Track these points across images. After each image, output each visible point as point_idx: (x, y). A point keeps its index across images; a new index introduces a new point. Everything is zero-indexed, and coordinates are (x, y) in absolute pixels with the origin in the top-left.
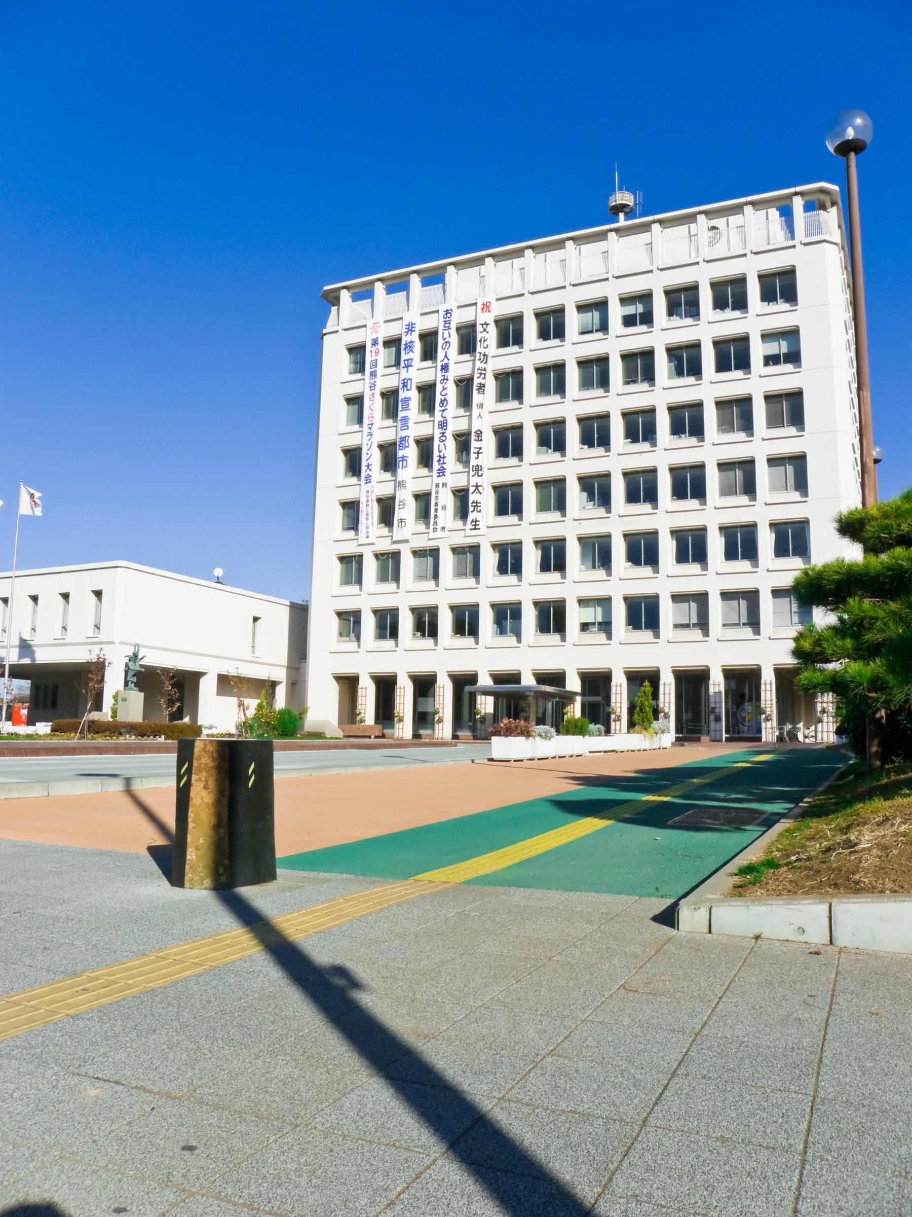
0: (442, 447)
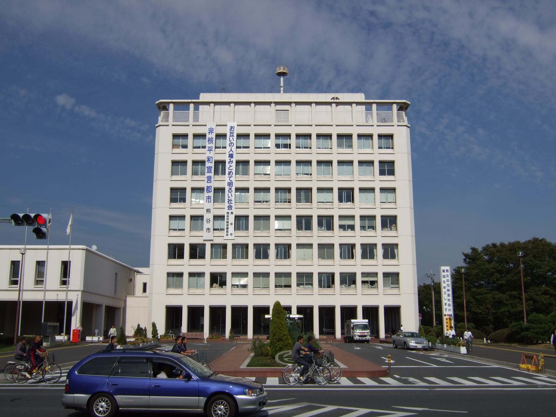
0: (230, 195)
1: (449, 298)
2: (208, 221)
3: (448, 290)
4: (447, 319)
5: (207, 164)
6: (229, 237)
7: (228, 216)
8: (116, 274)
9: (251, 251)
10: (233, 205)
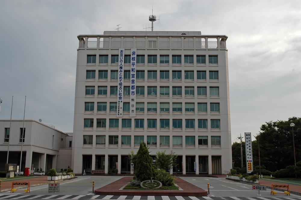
0: (120, 91)
1: (250, 151)
2: (133, 106)
3: (250, 146)
4: (249, 163)
5: (131, 73)
6: (120, 116)
7: (119, 103)
8: (53, 136)
9: (133, 123)
10: (122, 97)
